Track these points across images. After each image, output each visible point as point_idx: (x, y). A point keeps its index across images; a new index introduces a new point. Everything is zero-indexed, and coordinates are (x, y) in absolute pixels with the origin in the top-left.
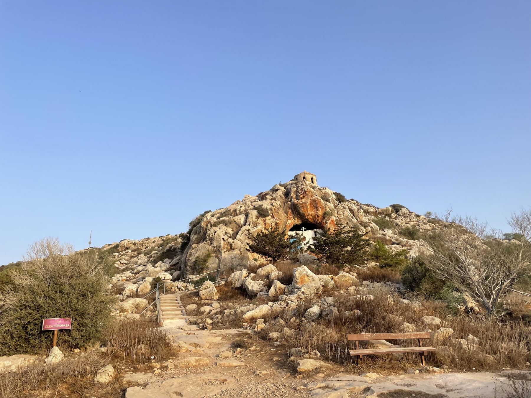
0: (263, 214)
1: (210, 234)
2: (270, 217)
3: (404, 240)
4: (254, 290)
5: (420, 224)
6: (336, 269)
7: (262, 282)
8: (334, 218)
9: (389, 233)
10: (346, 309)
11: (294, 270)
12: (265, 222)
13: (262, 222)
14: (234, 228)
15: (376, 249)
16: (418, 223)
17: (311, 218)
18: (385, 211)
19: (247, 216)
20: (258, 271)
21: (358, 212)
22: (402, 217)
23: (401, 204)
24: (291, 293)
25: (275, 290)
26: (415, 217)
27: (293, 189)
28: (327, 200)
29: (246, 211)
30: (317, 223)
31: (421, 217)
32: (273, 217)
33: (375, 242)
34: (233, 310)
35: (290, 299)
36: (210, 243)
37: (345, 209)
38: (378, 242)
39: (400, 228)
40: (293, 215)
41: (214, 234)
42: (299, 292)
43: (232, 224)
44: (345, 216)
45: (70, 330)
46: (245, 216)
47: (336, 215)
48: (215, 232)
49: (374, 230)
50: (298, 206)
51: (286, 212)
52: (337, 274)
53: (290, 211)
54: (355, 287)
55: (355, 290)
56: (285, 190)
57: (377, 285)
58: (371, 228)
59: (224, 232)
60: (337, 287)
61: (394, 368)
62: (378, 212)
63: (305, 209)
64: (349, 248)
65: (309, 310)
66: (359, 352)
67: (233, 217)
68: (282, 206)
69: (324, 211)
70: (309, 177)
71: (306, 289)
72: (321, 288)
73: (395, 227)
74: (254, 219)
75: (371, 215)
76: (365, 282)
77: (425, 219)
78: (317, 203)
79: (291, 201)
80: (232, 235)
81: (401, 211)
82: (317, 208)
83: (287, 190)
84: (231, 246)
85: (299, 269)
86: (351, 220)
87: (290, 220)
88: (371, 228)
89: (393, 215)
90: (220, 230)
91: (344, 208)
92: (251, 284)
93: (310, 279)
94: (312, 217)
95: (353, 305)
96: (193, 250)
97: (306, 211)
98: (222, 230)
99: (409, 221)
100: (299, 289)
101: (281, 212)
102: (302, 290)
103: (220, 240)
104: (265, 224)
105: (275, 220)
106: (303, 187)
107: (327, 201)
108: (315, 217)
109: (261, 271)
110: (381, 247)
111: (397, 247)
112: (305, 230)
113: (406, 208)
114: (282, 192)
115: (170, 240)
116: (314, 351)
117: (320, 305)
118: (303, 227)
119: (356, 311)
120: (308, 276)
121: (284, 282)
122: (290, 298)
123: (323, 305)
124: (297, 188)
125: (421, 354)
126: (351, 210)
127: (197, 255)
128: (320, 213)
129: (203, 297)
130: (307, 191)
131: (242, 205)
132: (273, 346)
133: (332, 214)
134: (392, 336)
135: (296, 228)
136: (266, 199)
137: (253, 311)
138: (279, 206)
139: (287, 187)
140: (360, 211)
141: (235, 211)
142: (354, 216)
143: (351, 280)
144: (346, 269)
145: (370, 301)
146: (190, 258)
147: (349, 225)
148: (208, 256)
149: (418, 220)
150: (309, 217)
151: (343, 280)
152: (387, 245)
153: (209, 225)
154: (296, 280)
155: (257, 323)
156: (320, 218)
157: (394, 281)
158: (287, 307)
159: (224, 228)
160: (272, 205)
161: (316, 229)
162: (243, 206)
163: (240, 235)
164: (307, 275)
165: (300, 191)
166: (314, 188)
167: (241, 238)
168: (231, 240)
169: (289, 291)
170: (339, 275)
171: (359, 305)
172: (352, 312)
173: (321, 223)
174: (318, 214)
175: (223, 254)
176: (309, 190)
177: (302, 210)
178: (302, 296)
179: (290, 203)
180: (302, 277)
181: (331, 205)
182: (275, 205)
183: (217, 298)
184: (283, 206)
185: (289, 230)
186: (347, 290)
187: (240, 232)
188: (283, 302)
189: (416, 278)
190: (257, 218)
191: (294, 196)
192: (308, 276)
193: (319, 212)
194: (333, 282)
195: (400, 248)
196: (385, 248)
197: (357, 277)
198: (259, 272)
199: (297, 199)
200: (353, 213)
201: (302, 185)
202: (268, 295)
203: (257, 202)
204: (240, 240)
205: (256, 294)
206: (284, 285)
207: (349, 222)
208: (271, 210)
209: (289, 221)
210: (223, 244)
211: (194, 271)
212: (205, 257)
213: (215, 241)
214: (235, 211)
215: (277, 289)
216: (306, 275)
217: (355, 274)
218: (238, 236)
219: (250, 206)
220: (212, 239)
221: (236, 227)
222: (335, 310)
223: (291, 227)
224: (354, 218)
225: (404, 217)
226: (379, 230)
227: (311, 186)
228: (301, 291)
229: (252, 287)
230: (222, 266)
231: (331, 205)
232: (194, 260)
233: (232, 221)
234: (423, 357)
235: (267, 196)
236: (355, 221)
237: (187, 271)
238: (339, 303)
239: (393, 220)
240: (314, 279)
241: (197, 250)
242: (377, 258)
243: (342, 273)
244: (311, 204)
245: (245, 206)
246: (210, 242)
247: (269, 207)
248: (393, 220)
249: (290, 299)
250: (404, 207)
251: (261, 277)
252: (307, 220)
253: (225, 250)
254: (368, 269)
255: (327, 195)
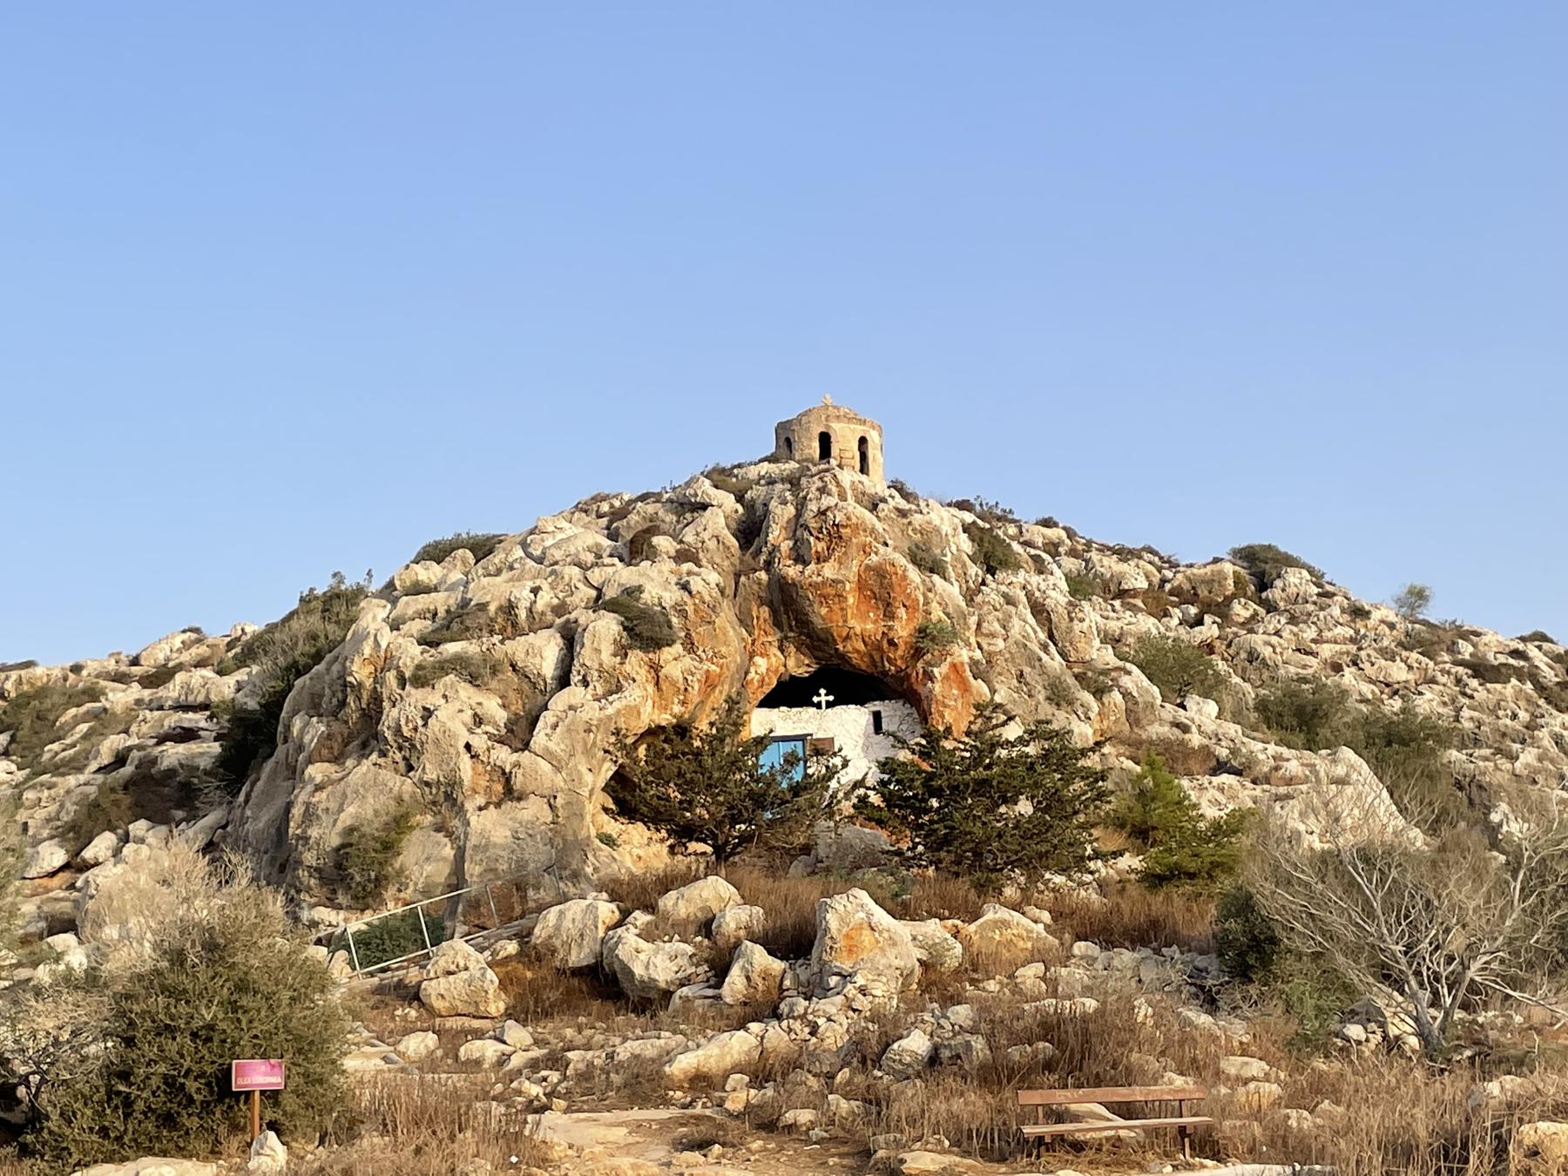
0: (645, 634)
1: (403, 722)
2: (677, 648)
3: (1263, 750)
4: (655, 980)
5: (1363, 654)
6: (972, 895)
7: (690, 949)
8: (962, 654)
9: (1202, 712)
10: (1016, 1040)
11: (825, 908)
12: (657, 672)
13: (642, 674)
14: (512, 695)
15: (1142, 794)
16: (1353, 648)
17: (858, 651)
18: (1203, 582)
19: (570, 638)
20: (661, 903)
21: (1071, 620)
22: (1283, 621)
23: (1282, 549)
24: (814, 989)
25: (748, 978)
26: (1347, 617)
27: (778, 511)
28: (934, 567)
29: (560, 609)
30: (885, 673)
31: (1376, 616)
32: (690, 646)
33: (1137, 764)
34: (597, 1053)
35: (821, 1013)
36: (402, 765)
37: (1014, 605)
38: (1151, 764)
39: (1266, 675)
40: (779, 635)
41: (420, 723)
42: (850, 990)
43: (500, 676)
44: (1010, 641)
45: (277, 1092)
46: (560, 641)
47: (973, 640)
48: (428, 713)
49: (1136, 703)
50: (801, 592)
51: (744, 620)
52: (975, 916)
53: (765, 612)
54: (1041, 966)
55: (1044, 979)
56: (741, 510)
57: (1125, 957)
58: (1126, 695)
59: (470, 712)
60: (975, 966)
61: (1118, 1164)
62: (1168, 586)
63: (836, 607)
64: (1025, 807)
65: (895, 1046)
66: (1047, 1129)
67: (502, 642)
68: (727, 592)
69: (919, 620)
70: (845, 441)
71: (870, 977)
72: (918, 971)
73: (1244, 670)
74: (607, 658)
75: (1134, 609)
76: (1080, 947)
77: (1392, 626)
78: (891, 585)
79: (768, 565)
80: (504, 731)
81: (1279, 583)
82: (889, 604)
83: (750, 507)
84: (508, 780)
85: (839, 902)
86: (1040, 660)
87: (762, 655)
88: (1126, 695)
89: (1241, 610)
90: (450, 705)
91: (1010, 601)
92: (642, 956)
93: (881, 939)
94: (865, 644)
95: (1034, 1027)
96: (323, 795)
97: (837, 616)
98: (458, 706)
99: (1313, 641)
100: (846, 977)
101: (726, 617)
102: (860, 980)
103: (452, 750)
104: (657, 684)
105: (701, 660)
106: (827, 501)
107: (932, 571)
108: (879, 649)
109: (676, 904)
110: (1163, 787)
111: (1230, 787)
112: (830, 705)
113: (1311, 571)
114: (726, 518)
115: (56, 698)
116: (937, 1136)
117: (929, 1029)
118: (822, 691)
119: (1041, 1045)
120: (873, 929)
121: (779, 950)
122: (822, 1007)
123: (939, 1031)
124: (801, 506)
125: (1182, 1130)
126: (1039, 610)
127: (345, 819)
128: (903, 630)
129: (438, 1004)
130: (846, 527)
131: (538, 582)
132: (808, 1142)
133: (955, 635)
134: (1121, 1094)
135: (789, 693)
136: (652, 555)
137: (700, 1052)
138: (716, 593)
139: (748, 496)
140: (1080, 615)
141: (509, 608)
142: (1051, 636)
143: (1029, 938)
144: (1010, 892)
145: (1085, 1018)
146: (314, 833)
147: (1027, 684)
148: (400, 824)
149: (1357, 632)
150: (849, 648)
151: (997, 937)
152: (1189, 774)
153: (391, 677)
154: (829, 942)
155: (728, 1088)
156: (900, 652)
157: (1193, 944)
158: (814, 1040)
159: (466, 693)
160: (685, 587)
161: (882, 699)
162: (545, 586)
163: (549, 731)
164: (870, 926)
165: (813, 524)
166: (874, 507)
167: (552, 745)
168: (503, 756)
169: (800, 984)
170: (981, 920)
171: (1049, 1028)
172: (1029, 1049)
173: (903, 677)
174: (891, 635)
175: (473, 819)
176: (854, 520)
177: (820, 614)
178: (862, 1003)
179: (763, 576)
180: (853, 933)
181: (951, 591)
182: (700, 589)
183: (502, 1011)
184: (730, 591)
185: (756, 702)
186: (1012, 976)
187: (547, 718)
188: (799, 1021)
189: (1262, 937)
190: (622, 652)
191: (786, 546)
192: (873, 929)
193: (897, 625)
194: (958, 949)
195: (1246, 794)
196: (1180, 787)
197: (1054, 927)
198: (669, 908)
199: (800, 559)
200: (1050, 621)
201: (823, 490)
202: (718, 997)
203: (610, 570)
204: (548, 756)
205: (667, 995)
206: (781, 959)
207: (1027, 670)
208: (683, 613)
209: (758, 659)
210: (470, 772)
211: (334, 891)
212: (386, 827)
213: (427, 755)
214: (509, 608)
215: (755, 977)
216: (866, 926)
217: (1046, 916)
218: (539, 738)
219: (580, 585)
220: (413, 746)
221: (519, 691)
222: (978, 1043)
223: (767, 690)
224: (1052, 648)
225: (1293, 620)
226: (1159, 701)
227: (863, 494)
228: (857, 985)
229: (647, 968)
230: (472, 870)
231: (951, 591)
232: (335, 841)
233: (501, 663)
234: (1186, 1140)
235: (656, 540)
236: (1054, 662)
237: (298, 891)
238: (990, 1023)
239: (1236, 635)
240: (897, 938)
241: (344, 795)
242: (1141, 834)
243: (993, 913)
244: (861, 585)
245: (553, 588)
246: (405, 758)
247: (671, 596)
248: (1236, 635)
249: (821, 1013)
250: (1291, 562)
251: (680, 929)
252: (843, 657)
253: (480, 800)
254: (1102, 886)
255: (935, 540)
